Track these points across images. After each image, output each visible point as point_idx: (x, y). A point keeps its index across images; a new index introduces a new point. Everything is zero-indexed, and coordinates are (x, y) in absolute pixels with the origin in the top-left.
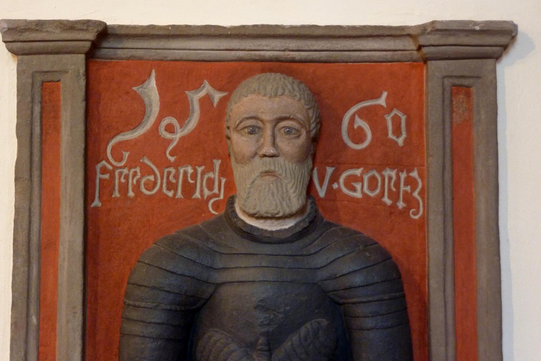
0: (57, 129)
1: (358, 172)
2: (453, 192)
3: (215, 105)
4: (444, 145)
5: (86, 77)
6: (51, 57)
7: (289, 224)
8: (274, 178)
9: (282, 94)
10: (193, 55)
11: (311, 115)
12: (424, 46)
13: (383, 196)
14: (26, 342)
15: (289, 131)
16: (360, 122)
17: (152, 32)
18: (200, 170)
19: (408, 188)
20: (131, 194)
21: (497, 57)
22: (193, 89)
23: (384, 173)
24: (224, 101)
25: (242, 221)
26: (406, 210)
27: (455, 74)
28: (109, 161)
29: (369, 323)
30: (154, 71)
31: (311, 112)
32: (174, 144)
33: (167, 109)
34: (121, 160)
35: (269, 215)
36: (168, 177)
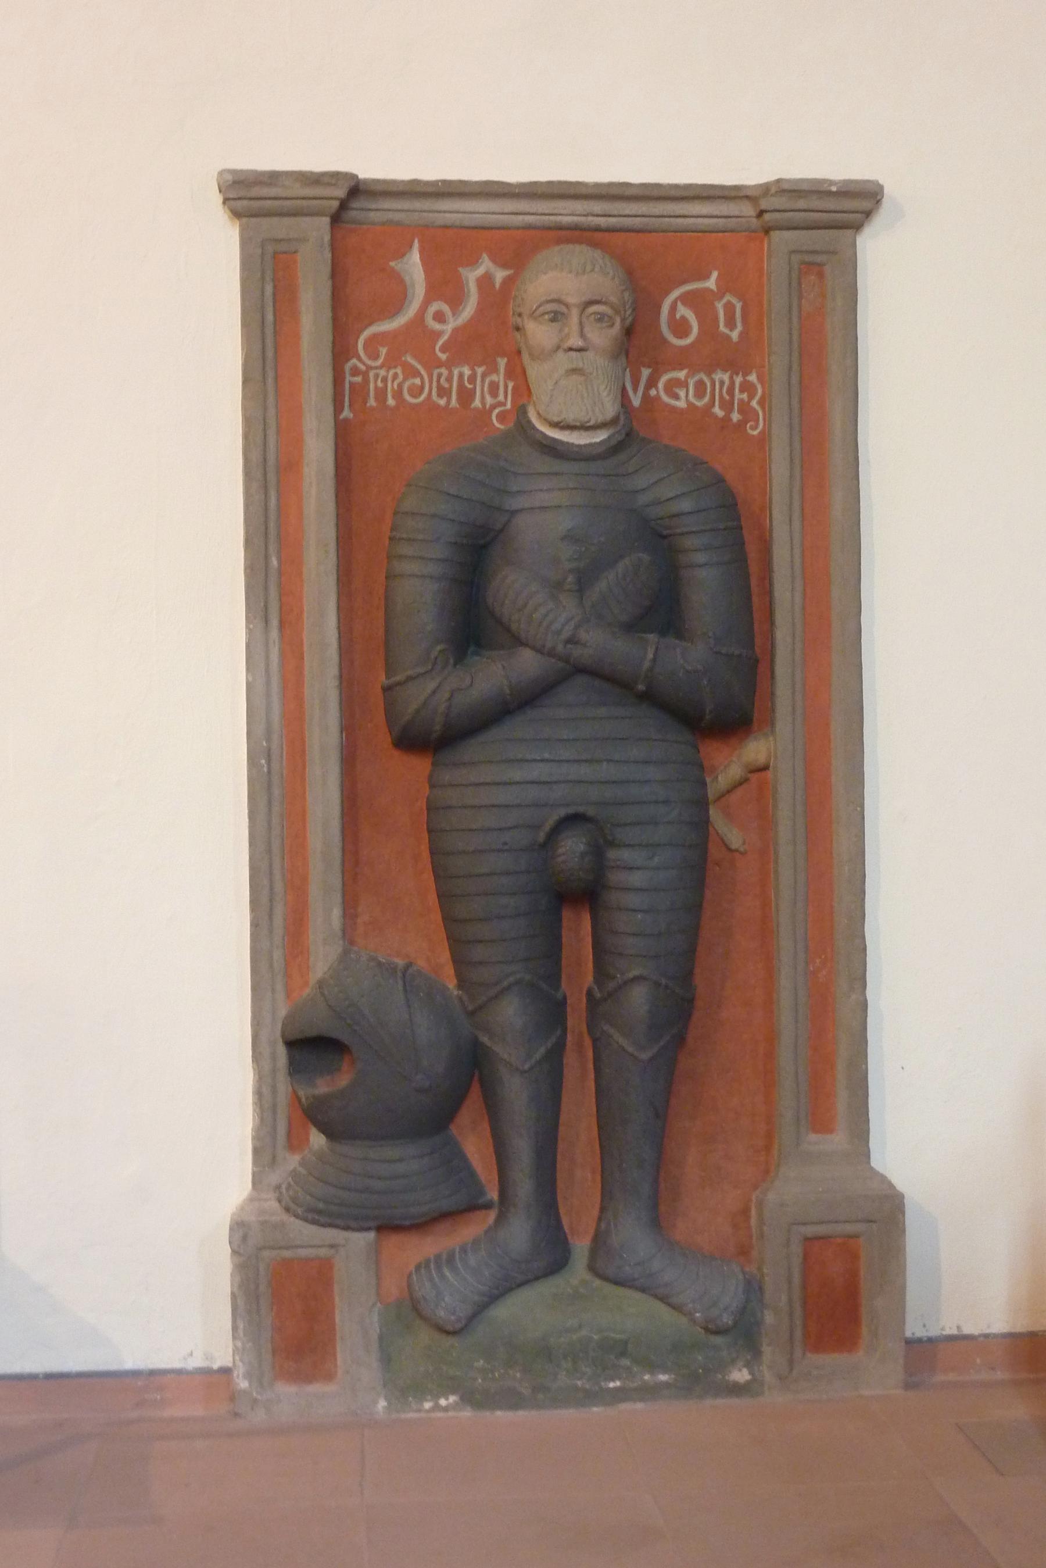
0: (295, 315)
1: (681, 375)
2: (801, 401)
3: (497, 286)
4: (791, 342)
5: (324, 250)
6: (286, 220)
7: (600, 436)
8: (583, 378)
9: (593, 270)
10: (468, 220)
11: (626, 299)
12: (766, 211)
13: (713, 405)
14: (266, 588)
15: (601, 318)
16: (683, 311)
17: (418, 189)
18: (480, 370)
19: (745, 396)
20: (391, 402)
21: (858, 227)
22: (467, 266)
23: (714, 376)
24: (508, 282)
25: (542, 433)
26: (741, 425)
27: (804, 248)
28: (361, 359)
29: (701, 558)
30: (416, 241)
31: (626, 294)
32: (445, 337)
33: (434, 292)
34: (376, 357)
35: (578, 424)
36: (438, 381)
